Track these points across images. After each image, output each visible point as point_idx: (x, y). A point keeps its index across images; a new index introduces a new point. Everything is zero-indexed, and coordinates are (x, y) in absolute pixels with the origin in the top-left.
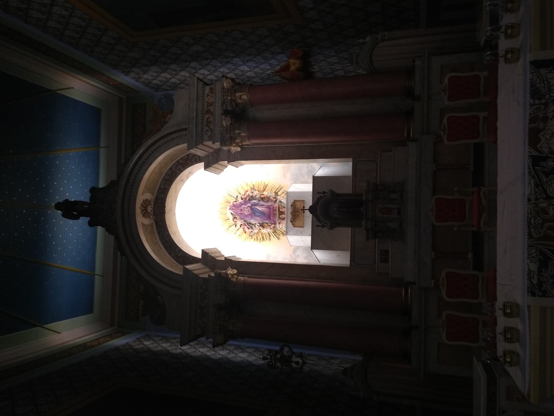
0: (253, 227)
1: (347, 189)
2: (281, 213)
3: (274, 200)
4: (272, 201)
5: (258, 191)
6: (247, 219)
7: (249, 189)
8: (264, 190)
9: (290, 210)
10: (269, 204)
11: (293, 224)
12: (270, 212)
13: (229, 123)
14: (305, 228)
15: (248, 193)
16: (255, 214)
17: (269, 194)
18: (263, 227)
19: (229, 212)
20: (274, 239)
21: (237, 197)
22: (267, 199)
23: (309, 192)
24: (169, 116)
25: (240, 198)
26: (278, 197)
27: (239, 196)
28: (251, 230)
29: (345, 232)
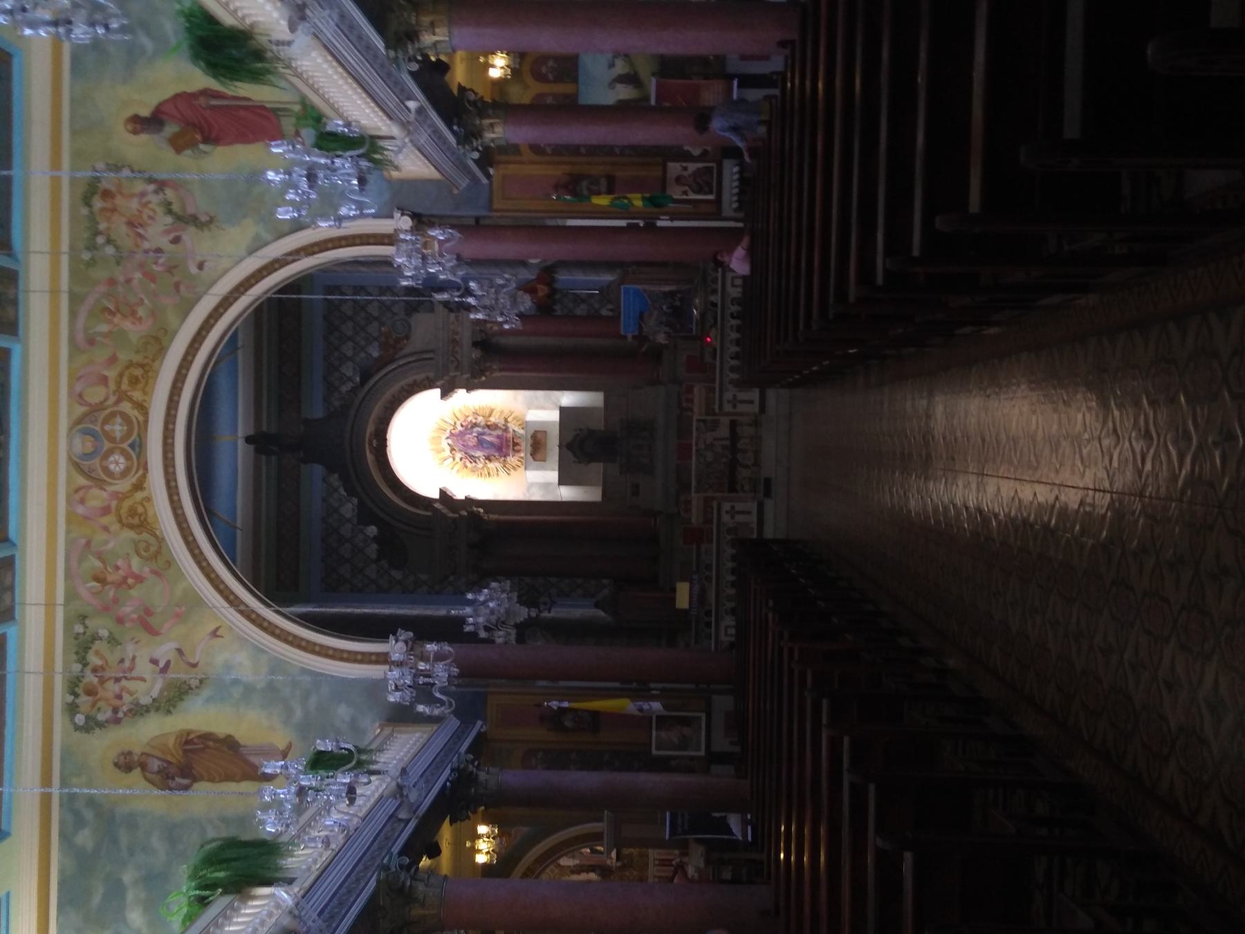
0: (477, 460)
1: (598, 424)
2: (515, 444)
3: (504, 427)
4: (501, 428)
5: (483, 416)
6: (469, 451)
7: (471, 413)
8: (490, 416)
9: (530, 441)
10: (499, 432)
11: (533, 458)
12: (502, 443)
13: (478, 356)
14: (547, 462)
15: (469, 419)
16: (482, 445)
17: (498, 421)
18: (490, 461)
19: (445, 444)
20: (502, 473)
21: (455, 423)
22: (493, 427)
23: (554, 422)
24: (405, 342)
25: (460, 425)
26: (509, 425)
27: (458, 423)
28: (474, 464)
29: (597, 468)
